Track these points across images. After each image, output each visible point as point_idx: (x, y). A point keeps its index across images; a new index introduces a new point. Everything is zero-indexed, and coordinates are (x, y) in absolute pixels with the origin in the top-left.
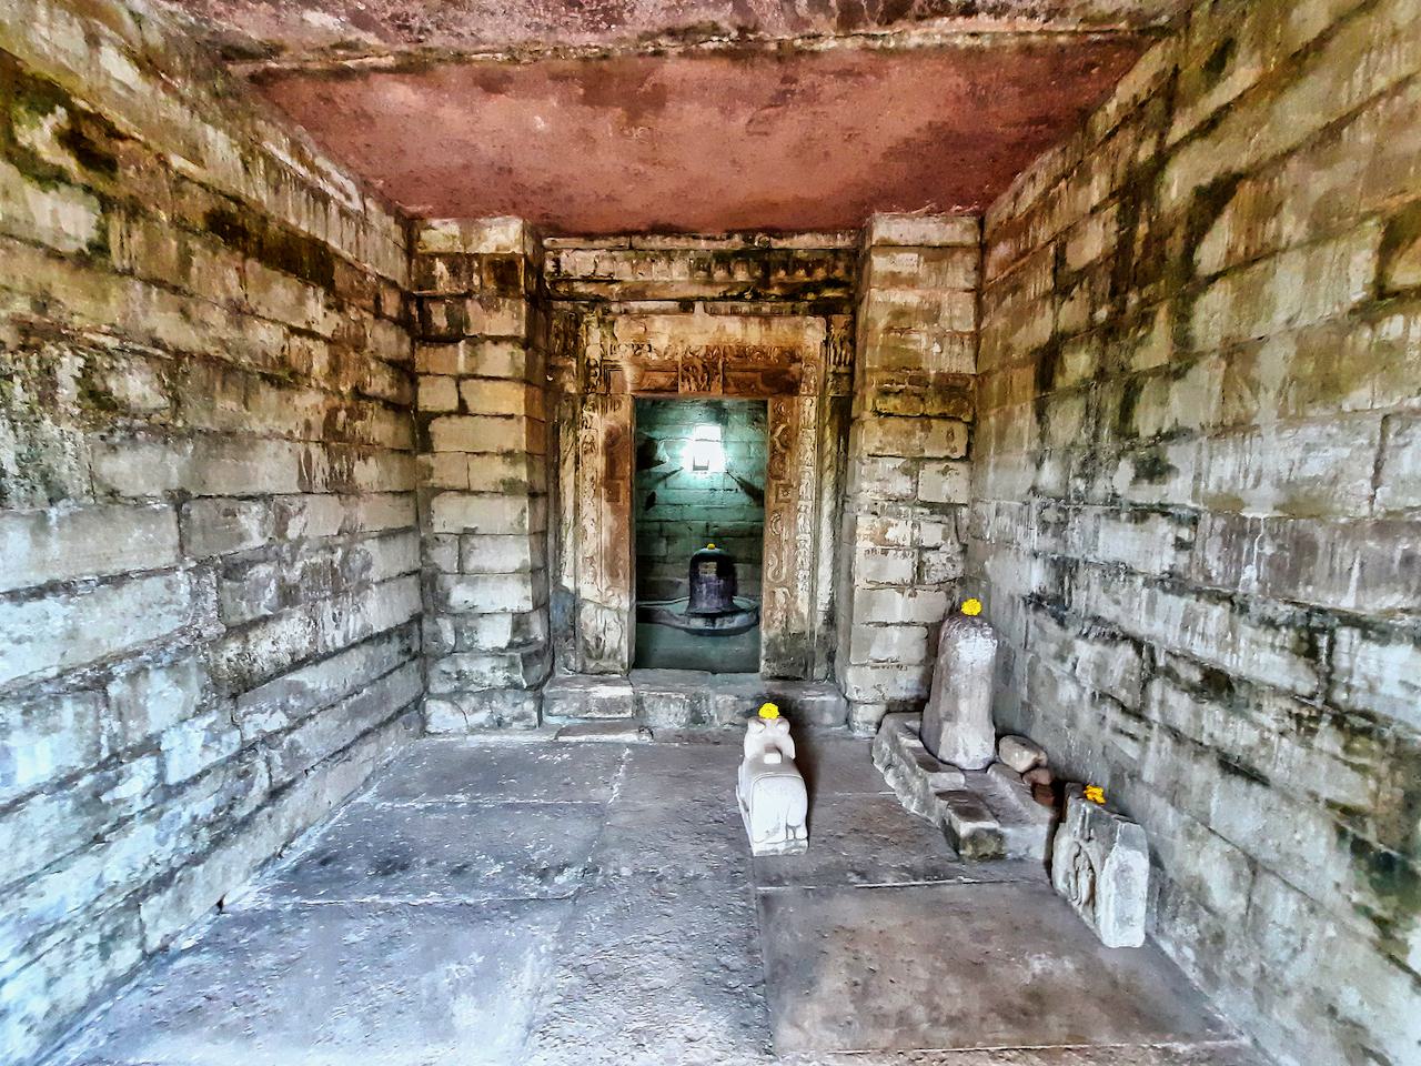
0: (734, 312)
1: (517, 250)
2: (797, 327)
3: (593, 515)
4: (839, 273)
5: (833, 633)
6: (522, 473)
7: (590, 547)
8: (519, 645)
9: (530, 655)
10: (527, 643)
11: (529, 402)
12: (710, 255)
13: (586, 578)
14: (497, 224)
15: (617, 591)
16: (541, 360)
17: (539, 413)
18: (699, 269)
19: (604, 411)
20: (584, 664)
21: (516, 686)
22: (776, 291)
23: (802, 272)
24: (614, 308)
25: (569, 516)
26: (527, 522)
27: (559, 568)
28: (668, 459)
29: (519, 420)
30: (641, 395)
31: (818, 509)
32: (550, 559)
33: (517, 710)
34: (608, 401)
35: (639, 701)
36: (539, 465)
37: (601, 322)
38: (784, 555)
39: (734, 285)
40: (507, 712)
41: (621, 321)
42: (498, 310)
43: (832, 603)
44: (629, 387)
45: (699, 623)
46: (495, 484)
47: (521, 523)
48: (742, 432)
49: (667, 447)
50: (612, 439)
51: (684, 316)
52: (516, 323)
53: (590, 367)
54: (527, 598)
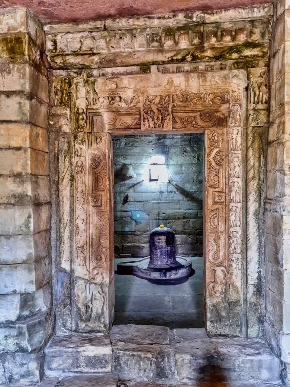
0: (179, 70)
1: (22, 29)
2: (225, 77)
3: (83, 216)
4: (256, 37)
5: (262, 301)
6: (28, 189)
7: (81, 239)
8: (26, 317)
9: (34, 325)
10: (33, 315)
11: (33, 138)
12: (161, 31)
13: (78, 261)
14: (9, 12)
15: (101, 270)
16: (43, 109)
17: (42, 144)
18: (153, 40)
19: (90, 144)
20: (77, 325)
21: (23, 350)
22: (209, 53)
23: (228, 38)
24: (95, 72)
25: (66, 218)
26: (32, 225)
27: (59, 255)
28: (135, 176)
29: (25, 151)
30: (115, 133)
31: (246, 208)
32: (53, 249)
33: (24, 369)
34: (93, 137)
35: (117, 359)
36: (43, 182)
37: (86, 82)
38: (222, 241)
39: (179, 52)
40: (16, 371)
41: (100, 81)
42: (9, 73)
43: (259, 278)
44: (107, 127)
45: (156, 275)
46: (8, 198)
47: (27, 226)
48: (177, 159)
49: (134, 169)
50: (96, 163)
51: (143, 76)
52: (22, 81)
53: (79, 114)
54: (31, 282)
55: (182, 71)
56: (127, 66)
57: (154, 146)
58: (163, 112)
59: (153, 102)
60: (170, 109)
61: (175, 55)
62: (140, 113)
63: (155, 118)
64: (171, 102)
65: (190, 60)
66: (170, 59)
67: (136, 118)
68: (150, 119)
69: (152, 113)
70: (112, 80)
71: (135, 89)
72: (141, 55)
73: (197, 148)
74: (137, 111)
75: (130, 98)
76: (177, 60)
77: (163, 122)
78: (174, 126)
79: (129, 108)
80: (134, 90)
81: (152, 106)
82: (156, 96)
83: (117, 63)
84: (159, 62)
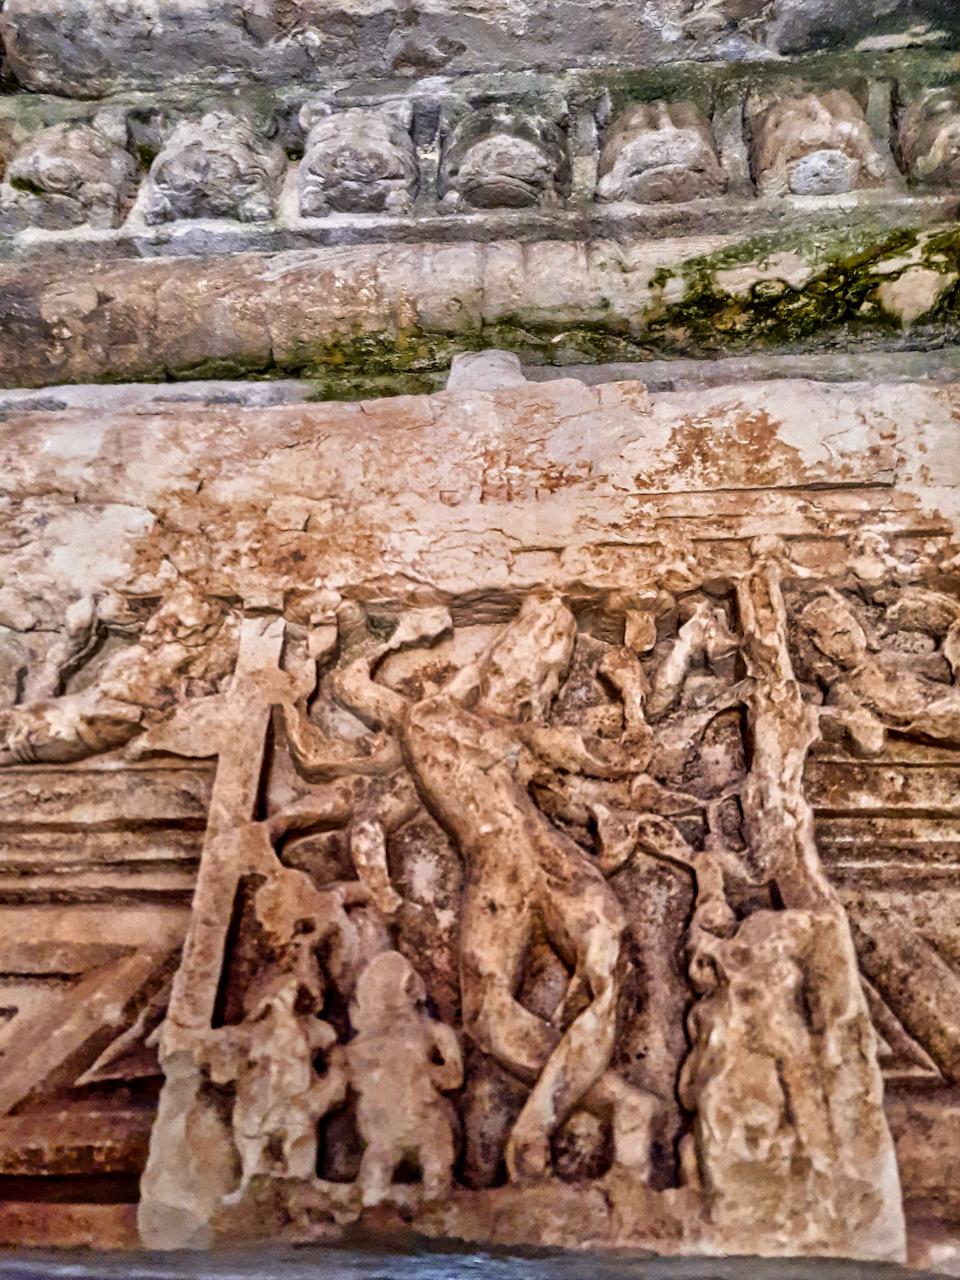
63: (493, 952)
64: (779, 688)
66: (676, 290)
67: (117, 954)
70: (81, 766)
76: (759, 304)
77: (657, 1044)
83: (46, 333)
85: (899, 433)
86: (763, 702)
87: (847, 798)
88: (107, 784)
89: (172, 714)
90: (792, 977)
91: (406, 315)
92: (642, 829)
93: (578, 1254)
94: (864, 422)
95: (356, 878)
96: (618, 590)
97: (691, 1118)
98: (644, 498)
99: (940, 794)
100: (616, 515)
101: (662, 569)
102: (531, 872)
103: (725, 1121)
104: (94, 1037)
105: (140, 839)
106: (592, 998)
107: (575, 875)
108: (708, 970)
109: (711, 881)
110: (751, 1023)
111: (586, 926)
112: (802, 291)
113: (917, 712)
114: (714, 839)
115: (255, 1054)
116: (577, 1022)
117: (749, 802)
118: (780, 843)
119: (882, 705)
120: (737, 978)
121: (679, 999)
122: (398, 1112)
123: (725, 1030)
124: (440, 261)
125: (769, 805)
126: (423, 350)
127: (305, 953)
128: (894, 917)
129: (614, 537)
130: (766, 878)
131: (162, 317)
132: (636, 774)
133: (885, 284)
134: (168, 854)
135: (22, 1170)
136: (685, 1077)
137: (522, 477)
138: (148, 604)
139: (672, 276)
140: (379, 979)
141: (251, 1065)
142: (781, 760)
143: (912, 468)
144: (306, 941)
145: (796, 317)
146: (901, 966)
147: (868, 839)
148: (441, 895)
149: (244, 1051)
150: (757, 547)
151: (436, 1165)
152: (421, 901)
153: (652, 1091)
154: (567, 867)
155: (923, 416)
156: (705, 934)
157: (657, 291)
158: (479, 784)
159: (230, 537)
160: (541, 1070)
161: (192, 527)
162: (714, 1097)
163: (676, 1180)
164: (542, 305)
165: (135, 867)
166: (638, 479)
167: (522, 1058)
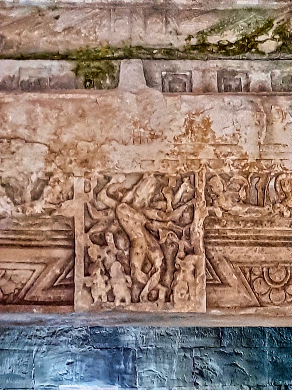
0: (227, 85)
55: (238, 89)
56: (22, 58)
57: (74, 349)
58: (170, 242)
59: (129, 196)
60: (198, 231)
61: (213, 30)
62: (72, 238)
63: (137, 263)
64: (201, 203)
65: (273, 49)
66: (194, 41)
67: (56, 260)
68: (115, 268)
69: (121, 242)
71: (56, 148)
72: (83, 21)
73: (250, 362)
74: (59, 232)
75: (34, 178)
77: (168, 278)
78: (214, 295)
79: (26, 218)
80: (51, 151)
81: (125, 213)
82: (141, 177)
84: (150, 51)
85: (241, 129)
86: (197, 206)
87: (213, 226)
88: (47, 221)
89: (61, 205)
90: (192, 268)
91: (105, 44)
92: (169, 235)
93: (152, 313)
94: (233, 124)
95: (107, 245)
96: (167, 173)
97: (172, 291)
98: (175, 145)
99: (233, 226)
100: (167, 150)
101: (178, 168)
102: (145, 246)
103: (177, 292)
104: (55, 276)
105: (56, 233)
106: (156, 271)
107: (154, 247)
108: (178, 266)
109: (181, 248)
110: (184, 276)
111: (156, 258)
112: (234, 44)
113: (230, 209)
114: (183, 238)
115: (95, 282)
116: (153, 276)
117: (191, 230)
118: (196, 240)
119: (223, 207)
120: (182, 268)
121: (173, 270)
122: (121, 291)
123: (180, 277)
124: (117, 27)
125: (195, 231)
126: (110, 52)
127: (100, 263)
128: (219, 252)
129: (167, 158)
130: (192, 246)
131: (23, 43)
132: (168, 221)
133: (259, 44)
134: (63, 237)
135: (47, 300)
136: (172, 284)
137: (144, 133)
138: (50, 175)
139: (193, 37)
140: (115, 267)
141: (94, 284)
142: (199, 221)
143: (243, 139)
144: (100, 260)
145: (233, 51)
146: (218, 262)
147: (217, 234)
148: (126, 248)
149: (92, 281)
150: (202, 162)
151: (128, 299)
152: (121, 250)
153: (167, 287)
154: (152, 245)
155: (248, 123)
156: (178, 259)
157: (188, 41)
158: (134, 227)
159: (68, 154)
160: (146, 284)
161: (57, 150)
162: (176, 289)
163: (169, 301)
164: (150, 44)
165: (55, 240)
166: (174, 138)
167: (143, 282)
